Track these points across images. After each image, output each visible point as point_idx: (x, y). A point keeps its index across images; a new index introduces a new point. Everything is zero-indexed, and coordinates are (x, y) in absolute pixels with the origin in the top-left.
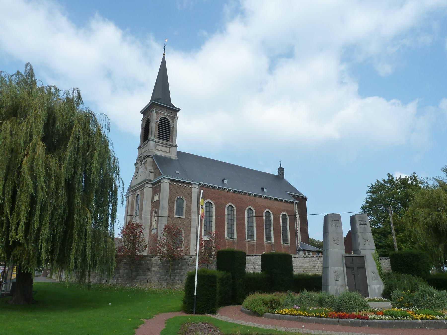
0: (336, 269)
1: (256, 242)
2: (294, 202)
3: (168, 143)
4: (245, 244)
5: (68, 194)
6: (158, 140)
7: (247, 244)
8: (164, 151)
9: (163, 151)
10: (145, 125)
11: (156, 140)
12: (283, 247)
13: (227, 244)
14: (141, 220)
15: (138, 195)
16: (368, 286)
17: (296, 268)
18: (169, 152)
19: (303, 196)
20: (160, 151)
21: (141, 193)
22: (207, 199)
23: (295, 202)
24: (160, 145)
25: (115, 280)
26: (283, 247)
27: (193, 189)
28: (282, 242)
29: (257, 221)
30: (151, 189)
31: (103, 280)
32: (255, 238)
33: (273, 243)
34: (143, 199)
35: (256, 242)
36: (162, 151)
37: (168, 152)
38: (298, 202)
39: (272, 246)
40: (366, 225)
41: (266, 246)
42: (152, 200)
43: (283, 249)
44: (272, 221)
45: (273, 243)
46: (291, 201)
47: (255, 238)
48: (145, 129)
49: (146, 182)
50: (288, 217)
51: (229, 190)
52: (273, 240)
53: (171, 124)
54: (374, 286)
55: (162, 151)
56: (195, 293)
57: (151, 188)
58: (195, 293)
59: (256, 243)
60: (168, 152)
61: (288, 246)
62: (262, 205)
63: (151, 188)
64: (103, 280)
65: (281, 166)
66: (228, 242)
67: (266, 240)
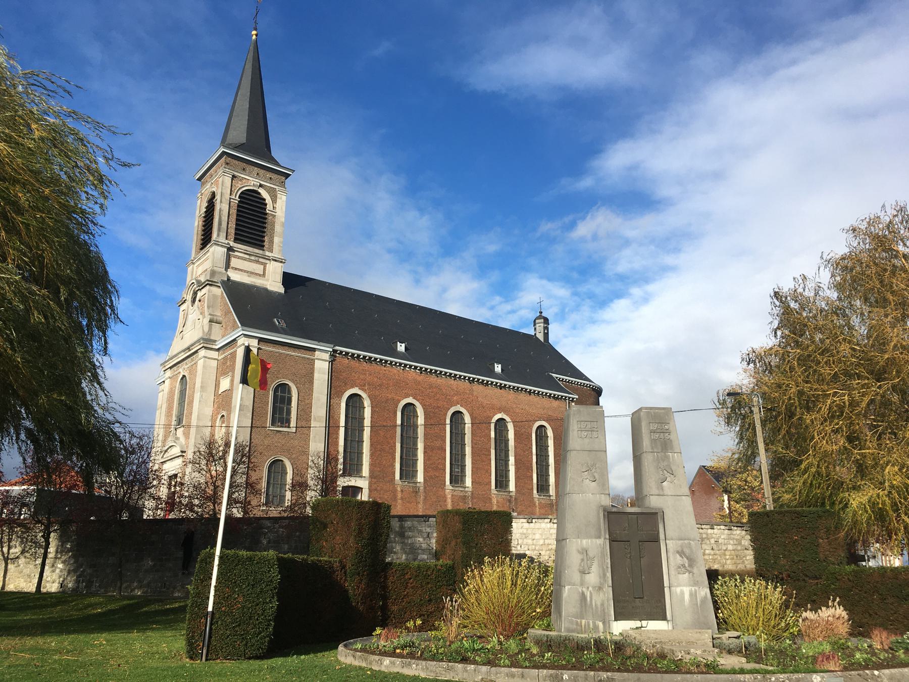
0: (585, 542)
1: (471, 490)
2: (566, 397)
3: (261, 252)
4: (445, 497)
5: (80, 395)
6: (236, 245)
7: (449, 496)
8: (252, 273)
9: (248, 272)
10: (207, 207)
11: (232, 244)
12: (537, 504)
13: (399, 495)
14: (189, 439)
15: (184, 376)
16: (665, 589)
17: (532, 550)
18: (264, 275)
19: (591, 383)
20: (242, 270)
21: (190, 373)
22: (352, 387)
23: (569, 398)
24: (239, 258)
25: (82, 583)
26: (537, 504)
27: (318, 364)
28: (535, 491)
29: (475, 441)
30: (214, 364)
31: (53, 582)
32: (468, 482)
33: (513, 494)
34: (194, 388)
35: (471, 490)
36: (245, 271)
37: (260, 275)
38: (577, 397)
39: (510, 501)
40: (667, 434)
41: (495, 502)
42: (503, 455)
43: (537, 508)
44: (511, 443)
45: (513, 494)
46: (558, 396)
47: (468, 482)
48: (205, 217)
49: (202, 345)
50: (550, 433)
51: (406, 365)
52: (512, 487)
53: (269, 207)
54: (682, 588)
55: (245, 271)
56: (210, 609)
57: (215, 359)
58: (210, 609)
59: (472, 494)
60: (260, 275)
61: (508, 497)
62: (489, 403)
63: (215, 359)
64: (54, 584)
65: (541, 313)
66: (402, 491)
67: (496, 487)
